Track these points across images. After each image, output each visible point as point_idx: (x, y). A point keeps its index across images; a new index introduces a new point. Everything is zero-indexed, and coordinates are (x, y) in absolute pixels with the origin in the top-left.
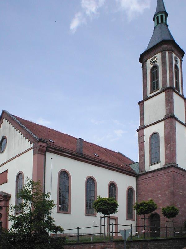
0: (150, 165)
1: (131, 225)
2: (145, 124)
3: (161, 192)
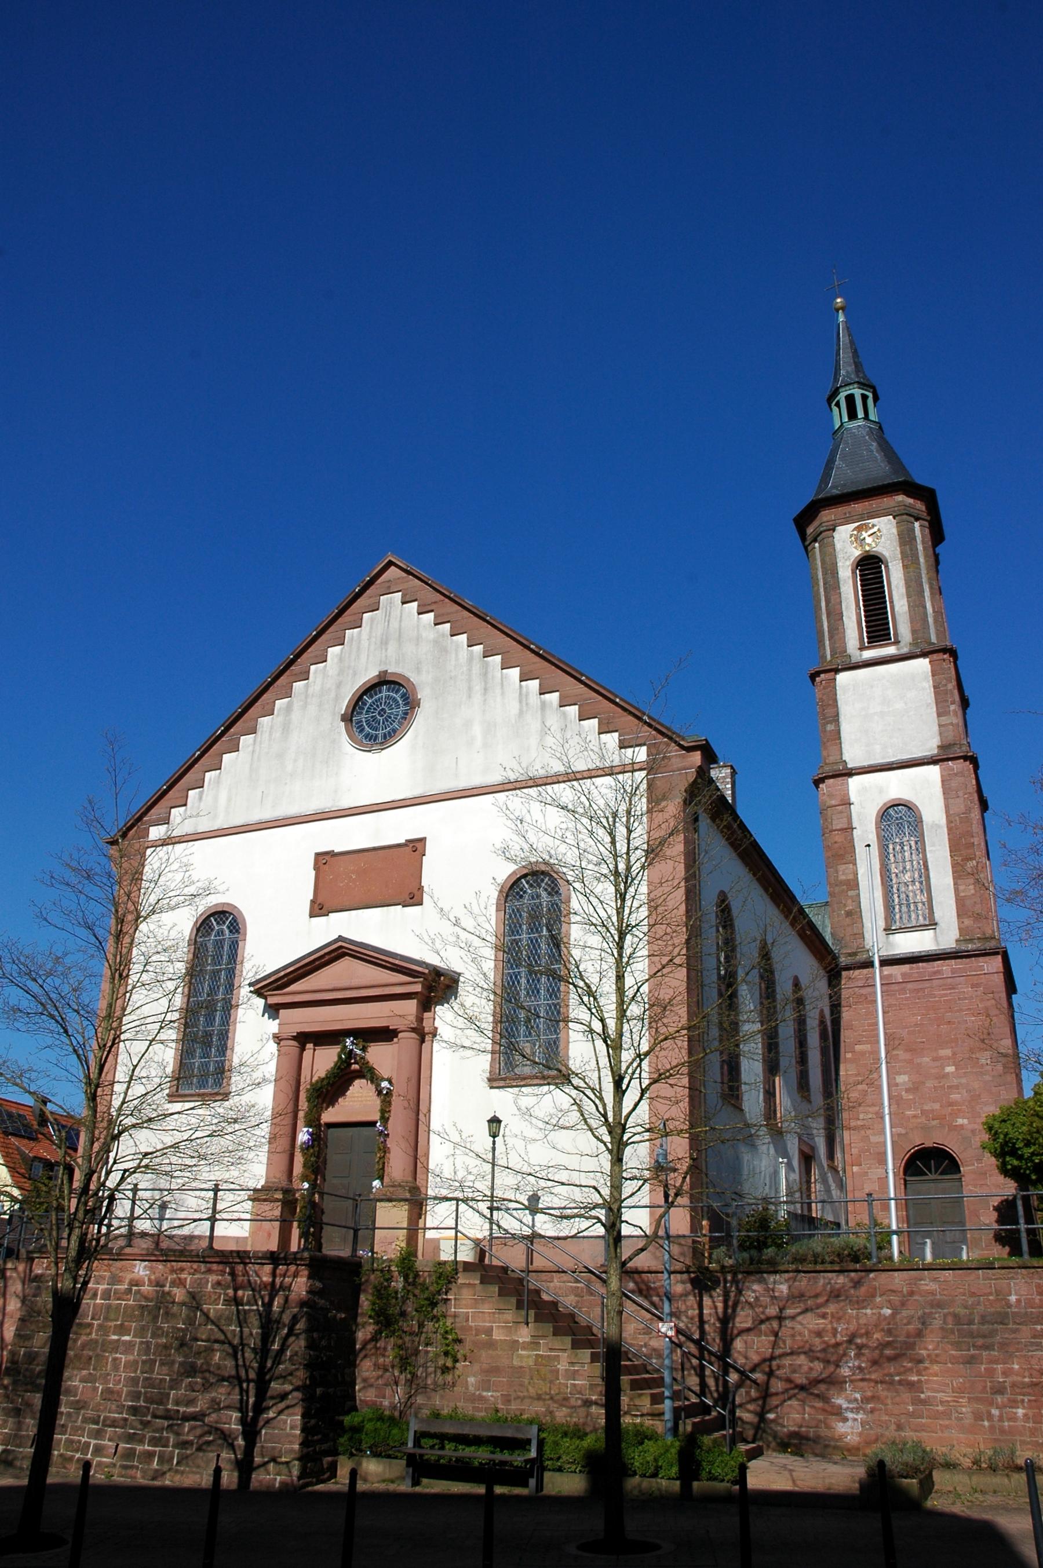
0: (888, 930)
1: (870, 1195)
2: (846, 757)
3: (954, 1054)
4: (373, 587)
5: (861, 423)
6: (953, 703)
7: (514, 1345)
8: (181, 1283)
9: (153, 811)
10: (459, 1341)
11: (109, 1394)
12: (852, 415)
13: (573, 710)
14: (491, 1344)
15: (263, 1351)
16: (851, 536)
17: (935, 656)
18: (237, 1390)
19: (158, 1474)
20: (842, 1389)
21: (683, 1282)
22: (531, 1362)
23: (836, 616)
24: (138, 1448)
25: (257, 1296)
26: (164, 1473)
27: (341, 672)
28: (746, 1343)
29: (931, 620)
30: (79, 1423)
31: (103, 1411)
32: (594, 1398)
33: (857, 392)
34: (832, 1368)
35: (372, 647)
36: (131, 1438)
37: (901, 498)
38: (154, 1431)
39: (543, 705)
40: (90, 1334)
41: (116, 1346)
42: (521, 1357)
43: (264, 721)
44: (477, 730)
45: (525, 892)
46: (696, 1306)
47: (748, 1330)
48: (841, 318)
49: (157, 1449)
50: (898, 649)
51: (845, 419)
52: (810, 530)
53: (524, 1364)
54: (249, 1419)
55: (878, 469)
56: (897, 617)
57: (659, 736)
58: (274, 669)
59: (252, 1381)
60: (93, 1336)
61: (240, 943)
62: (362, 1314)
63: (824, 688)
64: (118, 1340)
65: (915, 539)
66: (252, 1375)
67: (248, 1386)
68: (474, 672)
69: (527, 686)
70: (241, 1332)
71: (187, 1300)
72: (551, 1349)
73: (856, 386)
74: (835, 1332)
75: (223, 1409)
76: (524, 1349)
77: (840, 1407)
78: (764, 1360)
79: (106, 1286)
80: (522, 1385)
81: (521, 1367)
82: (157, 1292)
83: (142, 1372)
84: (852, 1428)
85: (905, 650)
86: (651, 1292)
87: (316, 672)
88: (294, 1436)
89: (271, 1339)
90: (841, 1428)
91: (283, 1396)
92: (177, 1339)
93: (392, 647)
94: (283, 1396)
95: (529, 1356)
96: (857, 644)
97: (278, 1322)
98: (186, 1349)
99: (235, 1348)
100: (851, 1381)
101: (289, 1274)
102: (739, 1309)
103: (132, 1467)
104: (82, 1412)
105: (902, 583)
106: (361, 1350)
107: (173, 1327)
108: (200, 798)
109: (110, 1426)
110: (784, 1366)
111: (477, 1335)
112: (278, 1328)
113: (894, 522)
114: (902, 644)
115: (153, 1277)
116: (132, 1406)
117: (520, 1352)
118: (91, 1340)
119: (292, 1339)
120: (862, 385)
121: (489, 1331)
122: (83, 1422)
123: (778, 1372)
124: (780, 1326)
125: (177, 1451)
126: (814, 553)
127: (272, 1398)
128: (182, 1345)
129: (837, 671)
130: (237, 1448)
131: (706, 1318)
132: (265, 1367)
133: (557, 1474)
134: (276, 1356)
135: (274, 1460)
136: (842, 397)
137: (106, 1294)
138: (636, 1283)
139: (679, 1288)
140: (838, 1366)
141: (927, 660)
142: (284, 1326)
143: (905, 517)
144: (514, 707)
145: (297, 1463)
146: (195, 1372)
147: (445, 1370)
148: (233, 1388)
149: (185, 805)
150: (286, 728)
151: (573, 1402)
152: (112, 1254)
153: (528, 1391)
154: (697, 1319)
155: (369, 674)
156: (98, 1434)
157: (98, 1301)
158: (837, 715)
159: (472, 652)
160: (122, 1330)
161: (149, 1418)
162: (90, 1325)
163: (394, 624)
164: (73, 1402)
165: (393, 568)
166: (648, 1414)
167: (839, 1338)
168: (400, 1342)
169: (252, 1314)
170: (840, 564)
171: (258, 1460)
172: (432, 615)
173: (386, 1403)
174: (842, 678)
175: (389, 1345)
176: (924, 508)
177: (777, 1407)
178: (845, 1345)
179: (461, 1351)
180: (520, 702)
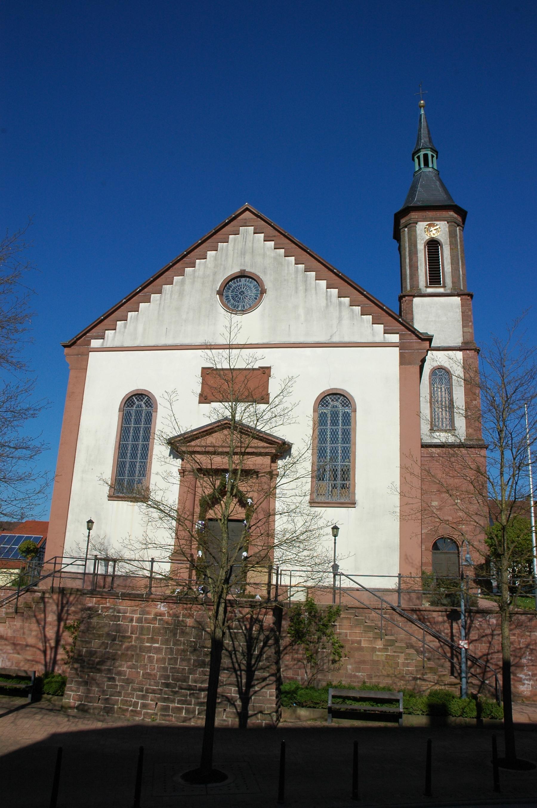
4: (235, 221)
5: (431, 170)
6: (471, 322)
7: (374, 649)
8: (191, 616)
9: (93, 330)
10: (342, 647)
11: (147, 676)
12: (426, 164)
13: (358, 309)
14: (361, 649)
15: (249, 654)
16: (425, 228)
17: (464, 297)
18: (234, 675)
19: (185, 720)
20: (523, 670)
21: (442, 616)
22: (383, 658)
23: (414, 268)
24: (171, 705)
25: (242, 624)
26: (190, 719)
27: (216, 266)
28: (475, 646)
29: (461, 278)
30: (129, 691)
31: (145, 685)
32: (418, 676)
33: (430, 153)
34: (517, 659)
35: (236, 255)
36: (165, 700)
37: (452, 213)
38: (181, 696)
39: (340, 303)
40: (131, 642)
41: (149, 650)
42: (378, 655)
43: (167, 288)
44: (301, 311)
45: (329, 403)
46: (449, 628)
47: (476, 640)
48: (422, 112)
49: (184, 706)
50: (445, 290)
51: (422, 165)
52: (403, 221)
53: (379, 659)
54: (244, 691)
55: (440, 197)
56: (446, 274)
57: (406, 330)
58: (174, 259)
59: (244, 670)
60: (133, 643)
61: (154, 414)
62: (284, 631)
63: (407, 304)
64: (151, 646)
65: (457, 235)
66: (243, 667)
67: (241, 673)
68: (299, 279)
69: (330, 291)
70: (233, 644)
71: (195, 626)
72: (395, 652)
73: (429, 149)
74: (519, 643)
75: (225, 685)
76: (379, 651)
77: (521, 678)
78: (484, 655)
79: (139, 616)
80: (378, 669)
81: (378, 661)
82: (175, 620)
83: (169, 664)
84: (527, 688)
85: (449, 291)
86: (426, 620)
87: (200, 263)
88: (272, 700)
89: (253, 648)
90: (522, 688)
91: (264, 679)
92: (191, 647)
93: (248, 257)
94: (264, 679)
95: (382, 655)
96: (424, 284)
97: (257, 639)
98: (197, 652)
99: (230, 652)
100: (527, 666)
101: (261, 613)
102: (471, 630)
103: (169, 715)
104: (131, 685)
105: (449, 257)
106: (283, 650)
107: (187, 640)
108: (125, 327)
109: (151, 693)
110: (494, 658)
111: (352, 644)
112: (257, 643)
113: (448, 225)
114: (447, 288)
115: (171, 612)
116: (165, 683)
117: (377, 653)
118: (132, 645)
119: (266, 648)
120: (433, 150)
121: (359, 642)
122: (131, 690)
123: (491, 661)
124: (492, 639)
125: (197, 708)
126: (404, 234)
127: (258, 680)
128: (195, 650)
129: (414, 296)
130: (237, 706)
131: (454, 634)
132: (251, 664)
133: (410, 716)
134: (257, 658)
135: (261, 712)
136: (421, 154)
137: (139, 620)
138: (418, 615)
139: (440, 619)
140: (521, 659)
141: (460, 298)
142: (261, 641)
143: (453, 223)
144: (323, 302)
145: (274, 714)
146: (205, 665)
147: (334, 661)
148: (231, 674)
149: (115, 329)
150: (181, 294)
151: (407, 677)
152: (143, 598)
153: (382, 672)
154: (450, 635)
155: (235, 270)
156: (143, 697)
157: (134, 624)
158: (413, 319)
159: (297, 268)
160: (153, 640)
161: (177, 689)
162: (130, 637)
163: (249, 244)
164: (123, 680)
165: (247, 212)
166: (448, 684)
167: (521, 646)
168: (307, 646)
169: (239, 634)
170: (418, 242)
171: (250, 712)
172: (273, 243)
173: (299, 678)
174: (416, 300)
175: (301, 647)
176: (461, 220)
177: (490, 677)
178: (524, 649)
179: (343, 652)
180: (327, 300)
